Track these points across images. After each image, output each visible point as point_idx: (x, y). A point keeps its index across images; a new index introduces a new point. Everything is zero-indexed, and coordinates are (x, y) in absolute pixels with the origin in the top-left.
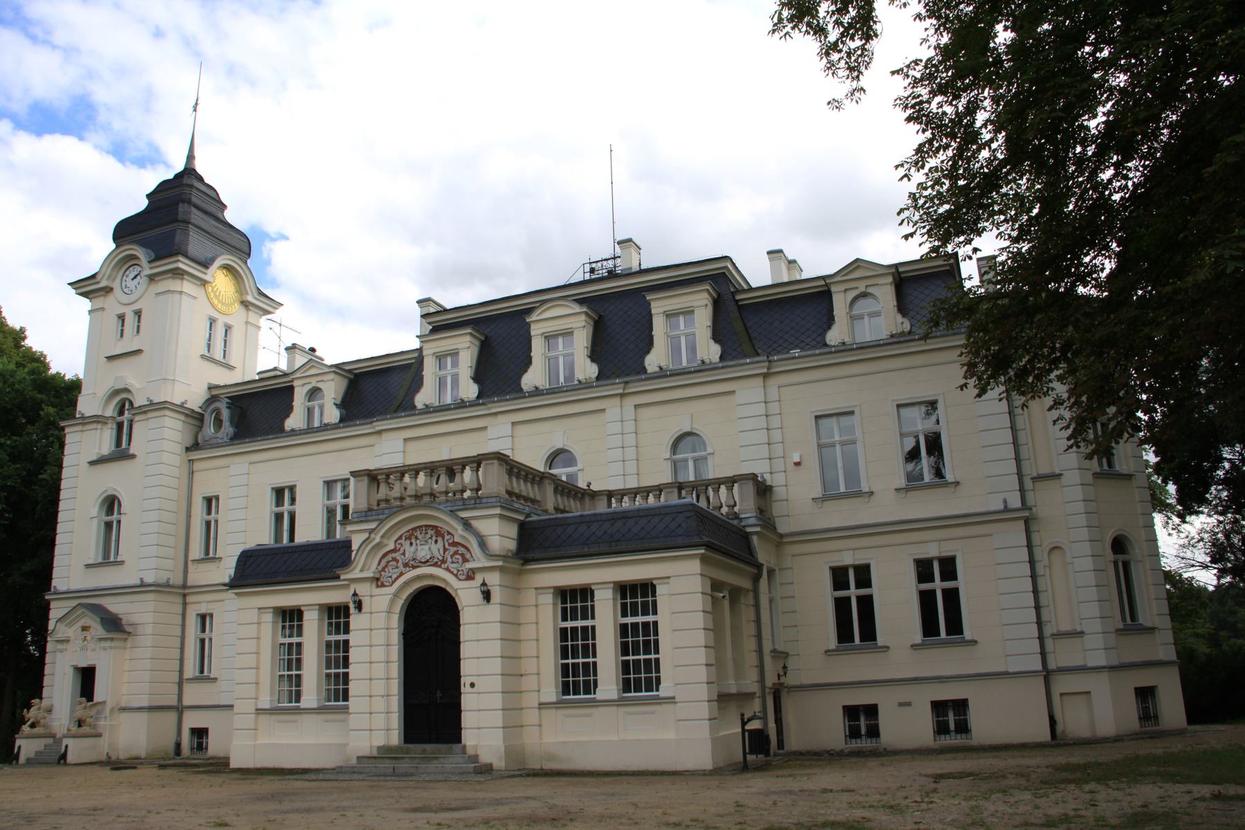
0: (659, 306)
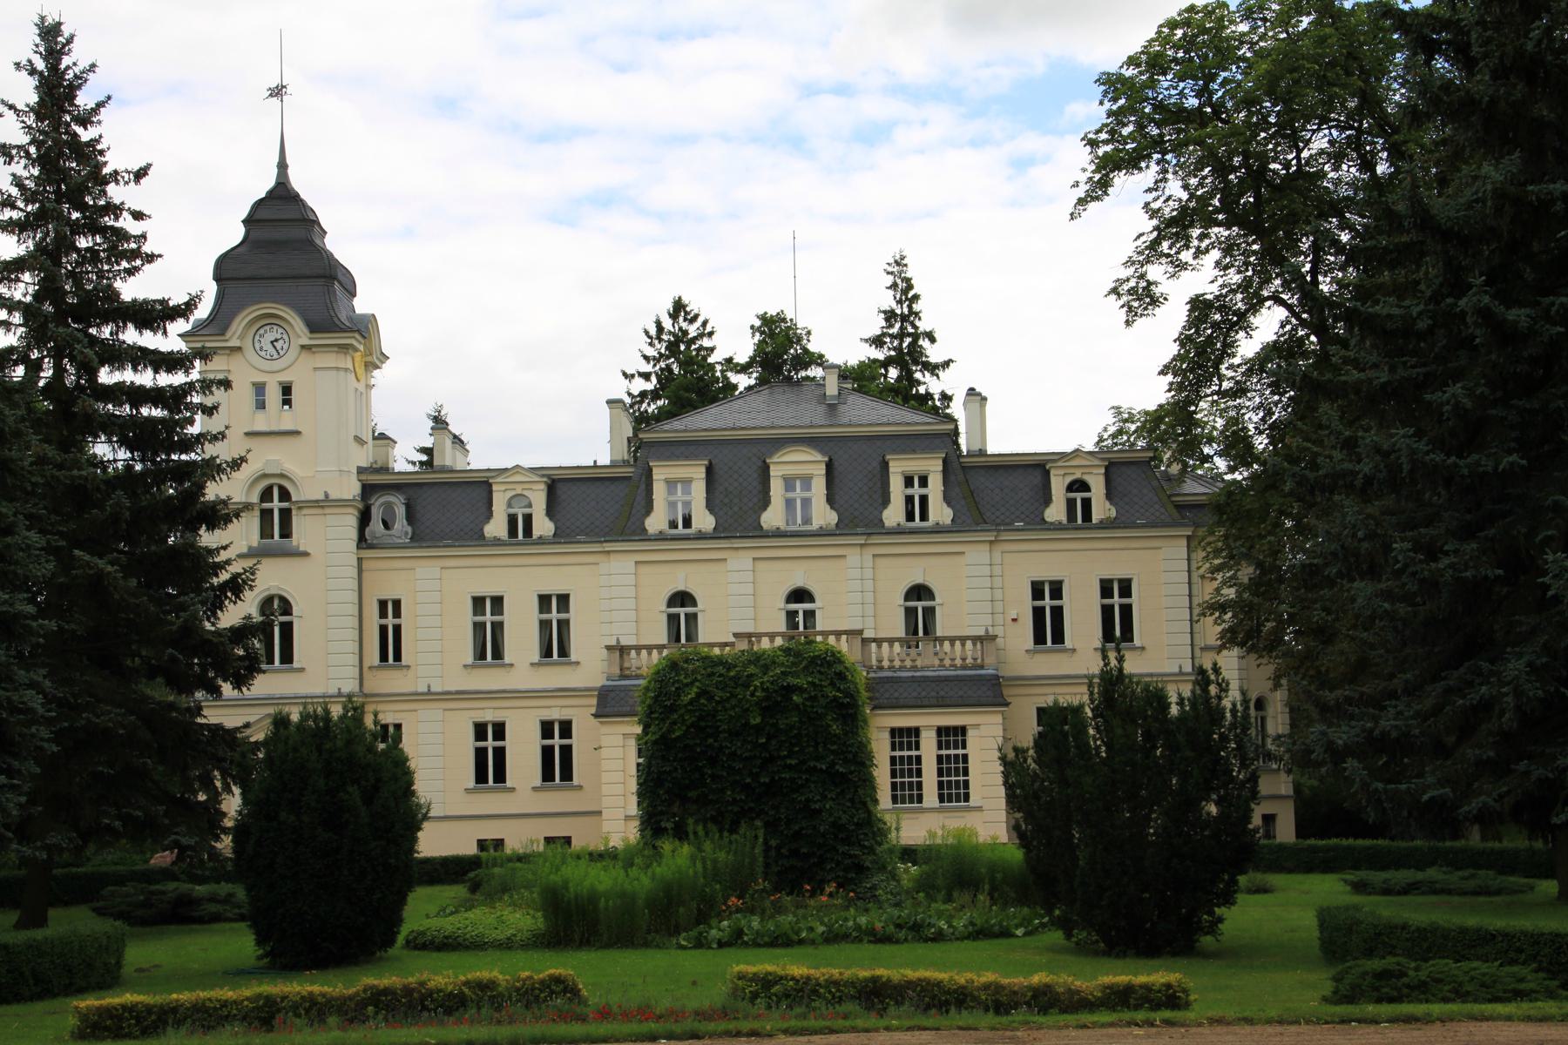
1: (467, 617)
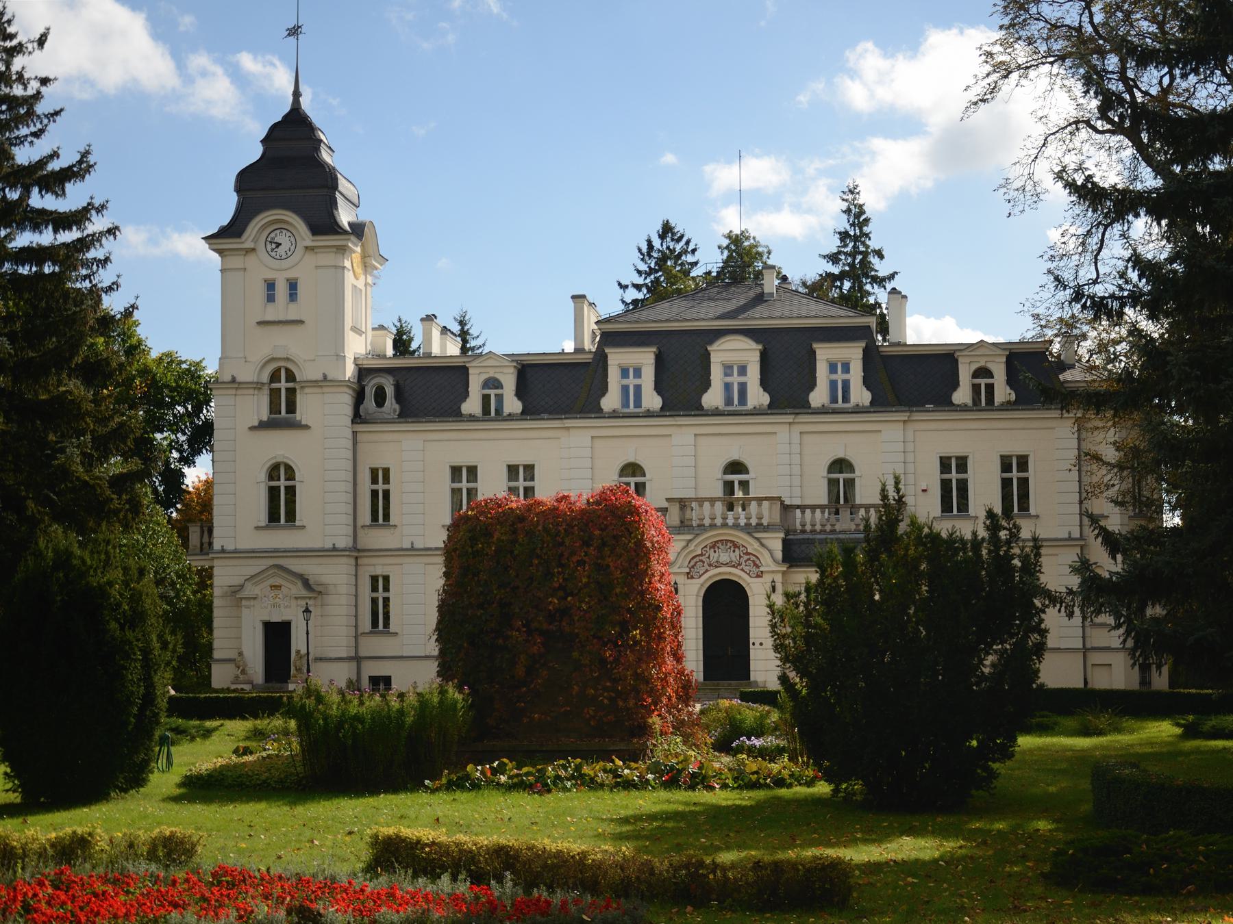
0: (825, 353)
1: (444, 484)
